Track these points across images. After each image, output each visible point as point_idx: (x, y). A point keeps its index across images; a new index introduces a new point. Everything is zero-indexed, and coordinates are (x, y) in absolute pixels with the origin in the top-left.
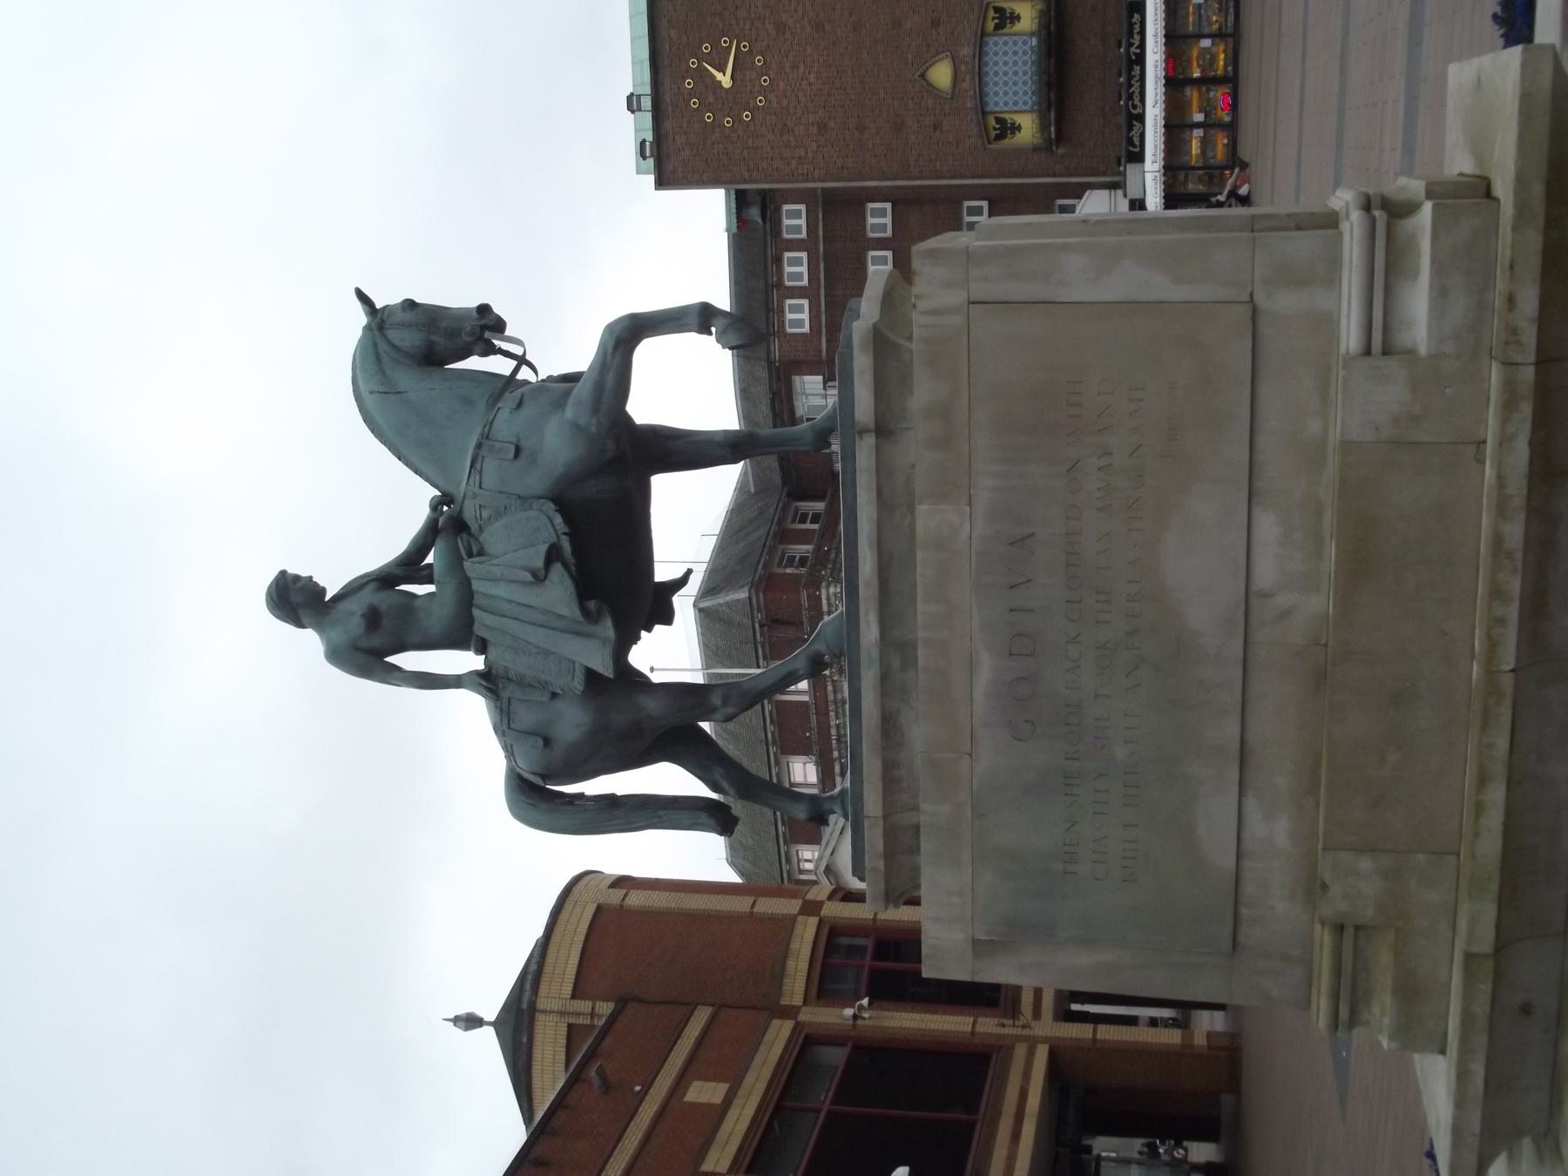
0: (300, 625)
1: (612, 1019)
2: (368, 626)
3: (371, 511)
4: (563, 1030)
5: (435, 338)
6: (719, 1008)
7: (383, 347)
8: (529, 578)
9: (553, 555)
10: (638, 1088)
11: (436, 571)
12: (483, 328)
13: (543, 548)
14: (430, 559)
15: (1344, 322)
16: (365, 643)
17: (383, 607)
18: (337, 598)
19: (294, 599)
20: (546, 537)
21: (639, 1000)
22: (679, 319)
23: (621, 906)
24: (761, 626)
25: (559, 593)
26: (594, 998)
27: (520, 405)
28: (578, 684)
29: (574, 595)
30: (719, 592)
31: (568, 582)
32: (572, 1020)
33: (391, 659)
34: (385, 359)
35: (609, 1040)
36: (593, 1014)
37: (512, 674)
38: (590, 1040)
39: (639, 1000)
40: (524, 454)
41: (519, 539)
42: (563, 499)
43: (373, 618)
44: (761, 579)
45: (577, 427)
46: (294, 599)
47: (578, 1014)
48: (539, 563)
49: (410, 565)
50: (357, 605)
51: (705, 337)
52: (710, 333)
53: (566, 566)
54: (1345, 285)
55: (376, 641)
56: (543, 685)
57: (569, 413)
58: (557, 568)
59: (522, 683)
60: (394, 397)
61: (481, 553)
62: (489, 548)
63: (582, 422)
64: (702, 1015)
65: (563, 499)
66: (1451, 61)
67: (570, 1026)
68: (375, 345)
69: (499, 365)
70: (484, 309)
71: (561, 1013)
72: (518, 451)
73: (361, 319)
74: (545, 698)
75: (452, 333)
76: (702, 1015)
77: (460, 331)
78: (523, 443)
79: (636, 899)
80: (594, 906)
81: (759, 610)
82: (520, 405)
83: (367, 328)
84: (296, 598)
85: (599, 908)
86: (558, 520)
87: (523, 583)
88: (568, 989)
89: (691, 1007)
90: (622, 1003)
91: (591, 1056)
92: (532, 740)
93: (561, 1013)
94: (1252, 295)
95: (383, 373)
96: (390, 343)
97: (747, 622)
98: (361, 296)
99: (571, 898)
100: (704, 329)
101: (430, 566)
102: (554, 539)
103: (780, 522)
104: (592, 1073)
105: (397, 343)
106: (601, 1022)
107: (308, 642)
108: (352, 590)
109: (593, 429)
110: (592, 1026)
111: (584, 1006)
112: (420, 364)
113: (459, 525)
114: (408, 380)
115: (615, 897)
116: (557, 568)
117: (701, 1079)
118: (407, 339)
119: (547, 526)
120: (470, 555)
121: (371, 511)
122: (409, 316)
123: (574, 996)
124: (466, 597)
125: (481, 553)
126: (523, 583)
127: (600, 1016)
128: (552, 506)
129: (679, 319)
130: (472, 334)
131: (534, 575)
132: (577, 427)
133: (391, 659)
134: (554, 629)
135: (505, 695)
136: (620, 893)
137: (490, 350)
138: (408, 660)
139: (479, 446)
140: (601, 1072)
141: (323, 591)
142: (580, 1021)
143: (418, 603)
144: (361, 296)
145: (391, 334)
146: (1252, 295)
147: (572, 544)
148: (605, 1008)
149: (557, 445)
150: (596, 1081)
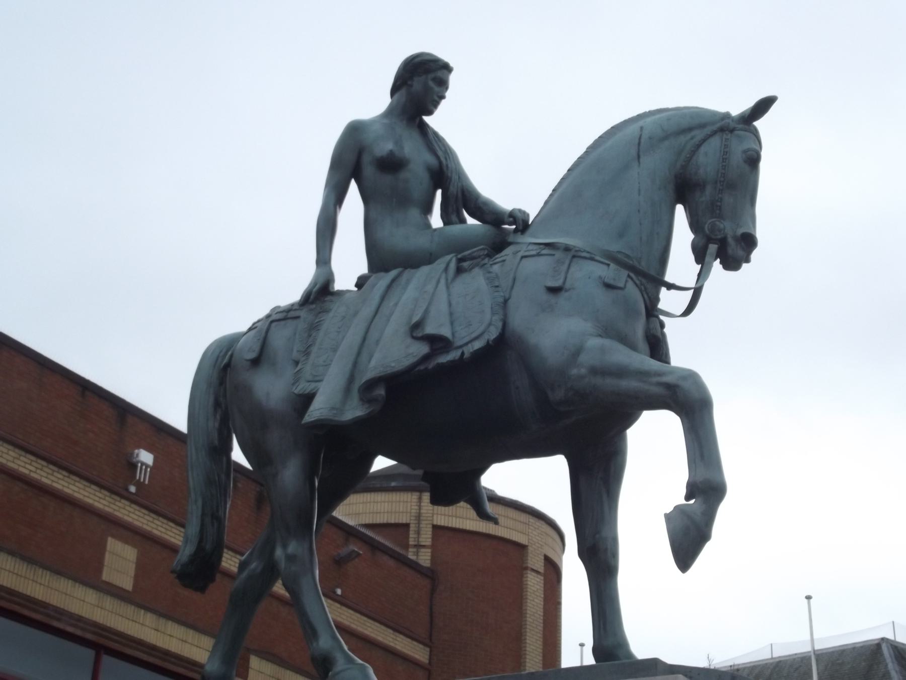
0: (394, 91)
1: (414, 566)
2: (394, 161)
3: (513, 149)
4: (403, 520)
5: (709, 190)
6: (427, 670)
7: (699, 135)
8: (415, 319)
9: (438, 343)
10: (339, 591)
11: (456, 228)
12: (728, 243)
13: (446, 332)
14: (471, 221)
16: (366, 159)
17: (404, 175)
18: (423, 128)
19: (421, 82)
20: (461, 335)
21: (433, 591)
22: (702, 456)
23: (526, 568)
26: (433, 547)
27: (609, 286)
28: (303, 387)
29: (389, 371)
30: (899, 663)
31: (406, 363)
32: (413, 528)
33: (353, 187)
34: (683, 139)
35: (391, 563)
36: (418, 546)
38: (387, 543)
39: (433, 591)
40: (552, 299)
41: (459, 308)
42: (503, 348)
43: (391, 165)
45: (578, 351)
46: (421, 82)
47: (418, 533)
48: (430, 329)
49: (462, 199)
50: (411, 148)
51: (684, 491)
52: (688, 498)
53: (426, 358)
55: (369, 171)
56: (307, 353)
57: (594, 342)
58: (423, 349)
59: (314, 327)
60: (634, 152)
61: (459, 271)
62: (465, 277)
63: (583, 358)
64: (419, 653)
65: (503, 349)
67: (407, 526)
68: (702, 126)
69: (681, 264)
71: (419, 517)
72: (554, 291)
73: (736, 105)
74: (295, 355)
75: (715, 209)
76: (419, 653)
77: (721, 217)
78: (564, 295)
79: (534, 584)
80: (521, 539)
82: (609, 286)
83: (727, 115)
84: (417, 84)
85: (522, 547)
86: (478, 345)
87: (410, 318)
89: (428, 642)
90: (430, 574)
91: (374, 546)
92: (257, 348)
93: (419, 517)
95: (666, 137)
96: (704, 140)
99: (532, 520)
100: (692, 491)
101: (463, 221)
102: (458, 343)
104: (353, 547)
105: (703, 149)
106: (411, 556)
107: (373, 101)
108: (432, 141)
109: (574, 371)
110: (406, 546)
111: (426, 538)
112: (676, 177)
113: (498, 245)
114: (657, 163)
115: (535, 561)
116: (423, 349)
118: (707, 160)
120: (460, 260)
121: (513, 149)
122: (737, 157)
123: (436, 528)
124: (412, 261)
125: (459, 271)
126: (410, 318)
127: (417, 554)
128: (493, 334)
129: (702, 456)
130: (713, 228)
131: (417, 326)
132: (578, 351)
133: (353, 187)
134: (359, 353)
135: (303, 313)
136: (539, 565)
137: (700, 254)
138: (353, 204)
139: (567, 249)
140: (353, 556)
141: (430, 113)
142: (412, 535)
143: (414, 213)
145: (715, 143)
147: (452, 362)
148: (424, 559)
149: (560, 334)
150: (344, 551)
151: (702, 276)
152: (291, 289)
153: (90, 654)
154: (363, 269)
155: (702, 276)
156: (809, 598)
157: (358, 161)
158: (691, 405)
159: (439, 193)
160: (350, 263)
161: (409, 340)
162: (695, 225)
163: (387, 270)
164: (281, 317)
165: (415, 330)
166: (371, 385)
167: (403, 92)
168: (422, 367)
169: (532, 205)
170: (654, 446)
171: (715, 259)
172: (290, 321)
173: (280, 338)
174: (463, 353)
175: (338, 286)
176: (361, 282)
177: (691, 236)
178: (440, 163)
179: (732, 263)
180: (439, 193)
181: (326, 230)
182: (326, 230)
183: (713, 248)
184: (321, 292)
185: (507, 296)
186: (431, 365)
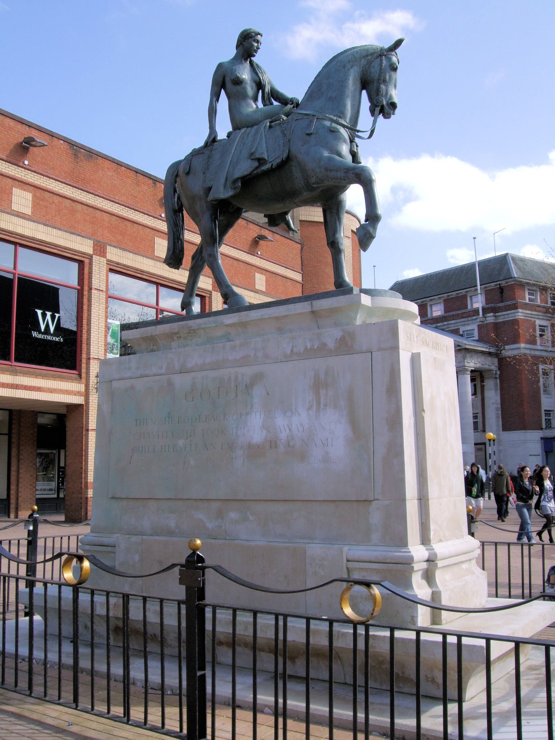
0: (238, 47)
14: (275, 103)
15: (364, 547)
16: (228, 80)
24: (499, 284)
25: (245, 168)
37: (214, 152)
44: (520, 282)
46: (247, 44)
48: (258, 156)
53: (257, 168)
54: (385, 548)
55: (229, 84)
58: (256, 164)
59: (209, 157)
66: (186, 605)
68: (372, 54)
70: (393, 106)
78: (313, 136)
81: (507, 283)
86: (279, 160)
88: (303, 218)
94: (377, 499)
97: (501, 278)
98: (398, 43)
101: (272, 104)
103: (528, 284)
107: (229, 52)
117: (267, 281)
118: (374, 71)
119: (273, 158)
120: (271, 122)
128: (285, 155)
131: (252, 154)
138: (223, 102)
144: (398, 43)
146: (377, 499)
151: (375, 122)
152: (200, 143)
153: (12, 247)
154: (230, 129)
155: (375, 122)
156: (374, 266)
157: (224, 81)
158: (366, 181)
159: (260, 91)
160: (223, 128)
161: (250, 161)
162: (370, 99)
163: (240, 129)
164: (195, 153)
165: (251, 156)
166: (235, 181)
167: (241, 47)
168: (255, 172)
169: (300, 95)
170: (353, 197)
171: (380, 114)
172: (200, 155)
173: (198, 163)
174: (272, 165)
175: (219, 138)
176: (229, 135)
177: (369, 104)
178: (260, 79)
179: (387, 116)
180: (260, 91)
181: (212, 112)
182: (212, 112)
183: (378, 109)
184: (212, 141)
185: (23, 524)
186: (259, 171)
